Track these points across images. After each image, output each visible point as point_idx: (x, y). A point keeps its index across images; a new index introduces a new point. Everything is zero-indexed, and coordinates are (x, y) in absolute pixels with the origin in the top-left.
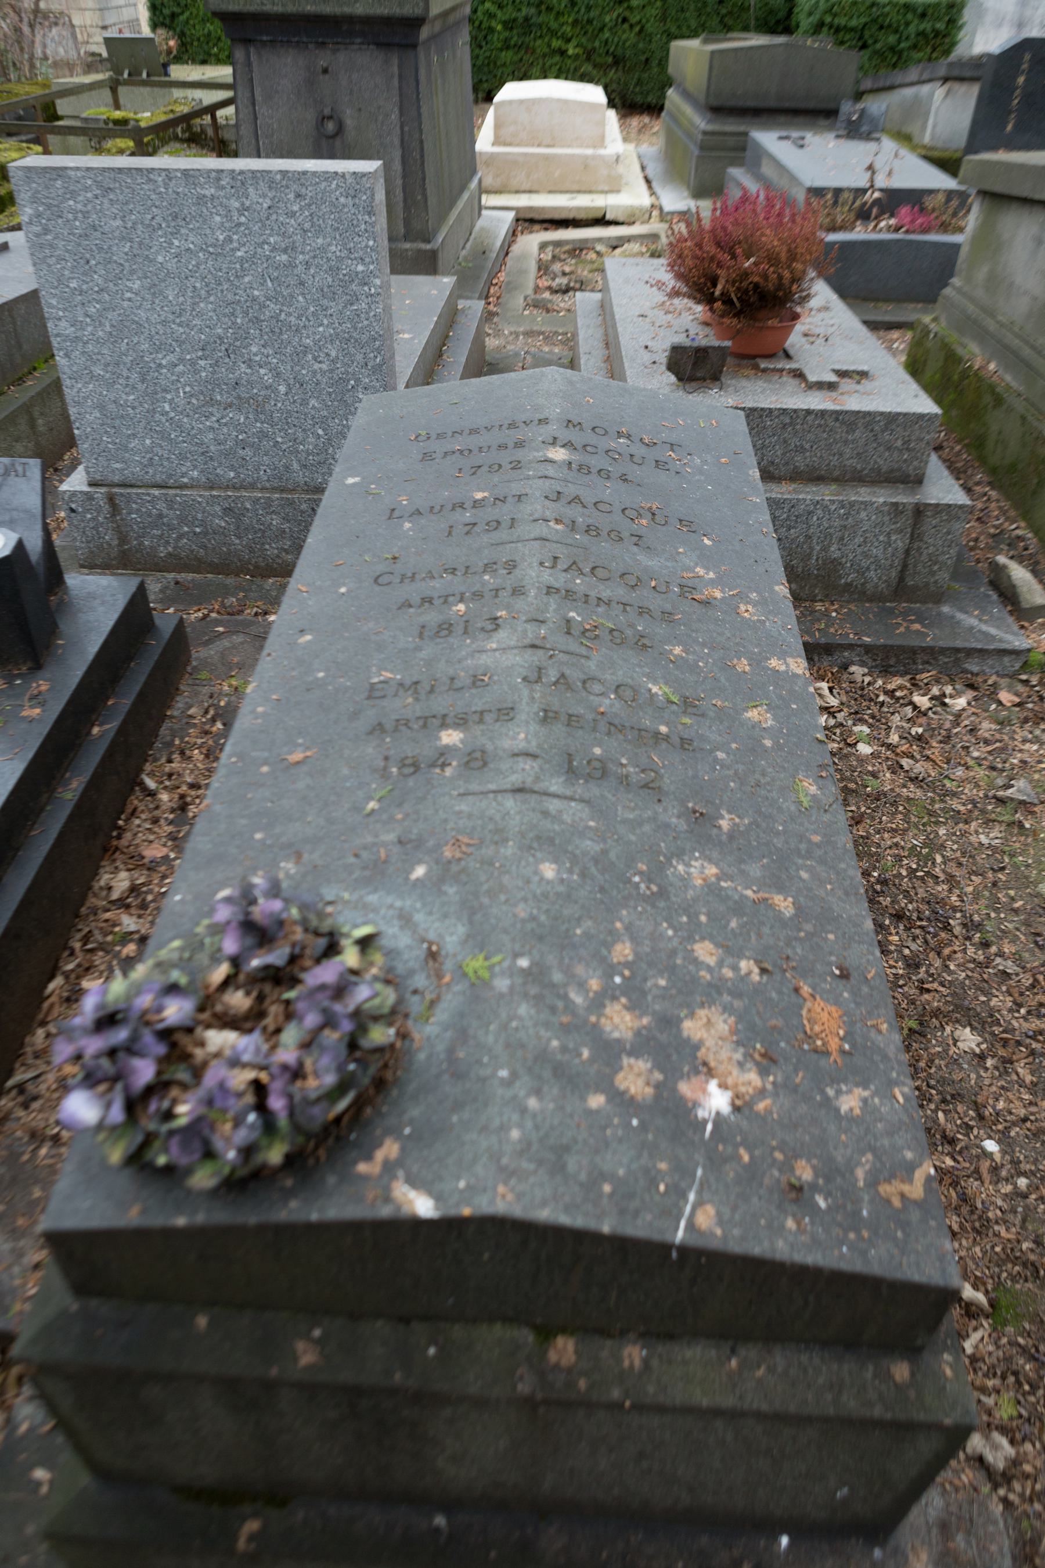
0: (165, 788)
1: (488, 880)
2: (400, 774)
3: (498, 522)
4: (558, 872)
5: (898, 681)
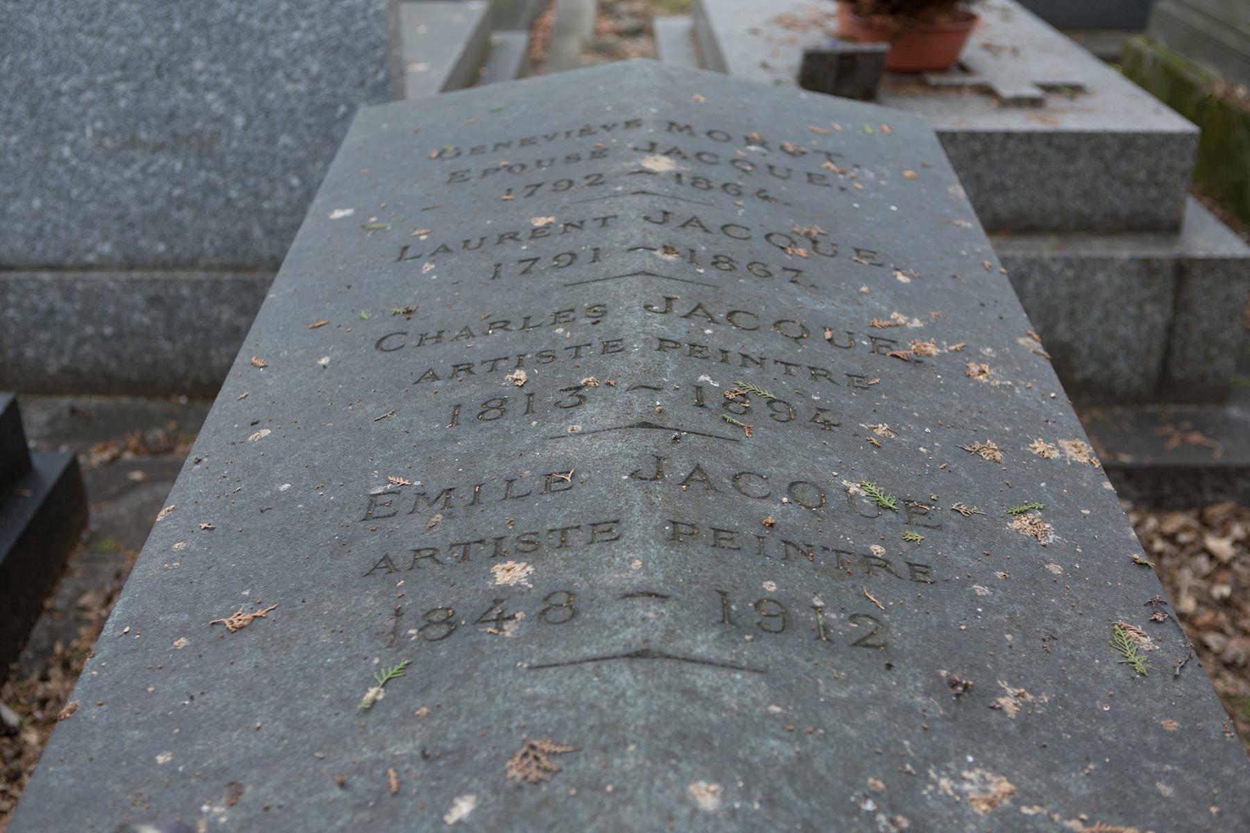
0: (35, 723)
1: (593, 819)
2: (423, 637)
3: (573, 256)
4: (724, 797)
5: (1175, 522)
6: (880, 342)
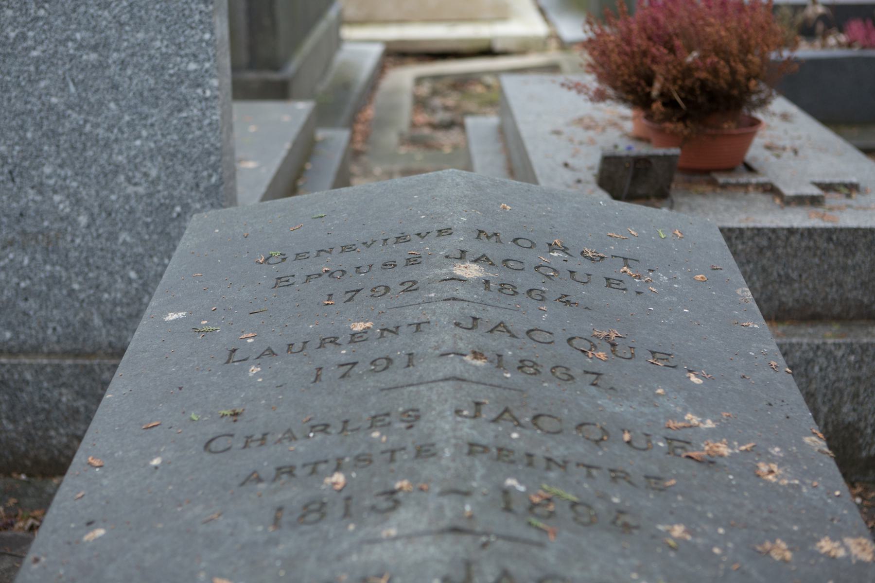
3: (389, 360)
6: (676, 444)
